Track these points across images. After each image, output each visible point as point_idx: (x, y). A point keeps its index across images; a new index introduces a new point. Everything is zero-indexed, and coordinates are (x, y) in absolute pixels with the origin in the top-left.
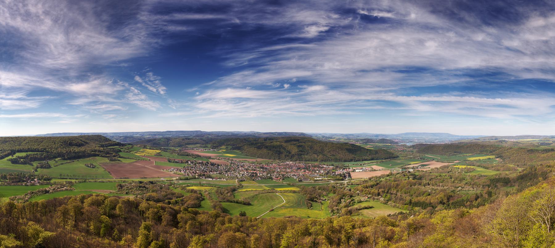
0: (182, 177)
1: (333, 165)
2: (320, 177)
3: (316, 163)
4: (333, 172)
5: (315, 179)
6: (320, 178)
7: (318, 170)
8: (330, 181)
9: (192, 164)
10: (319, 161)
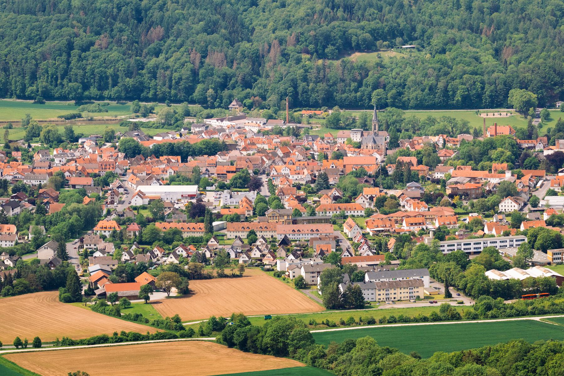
2: (538, 256)
5: (493, 275)
6: (536, 273)
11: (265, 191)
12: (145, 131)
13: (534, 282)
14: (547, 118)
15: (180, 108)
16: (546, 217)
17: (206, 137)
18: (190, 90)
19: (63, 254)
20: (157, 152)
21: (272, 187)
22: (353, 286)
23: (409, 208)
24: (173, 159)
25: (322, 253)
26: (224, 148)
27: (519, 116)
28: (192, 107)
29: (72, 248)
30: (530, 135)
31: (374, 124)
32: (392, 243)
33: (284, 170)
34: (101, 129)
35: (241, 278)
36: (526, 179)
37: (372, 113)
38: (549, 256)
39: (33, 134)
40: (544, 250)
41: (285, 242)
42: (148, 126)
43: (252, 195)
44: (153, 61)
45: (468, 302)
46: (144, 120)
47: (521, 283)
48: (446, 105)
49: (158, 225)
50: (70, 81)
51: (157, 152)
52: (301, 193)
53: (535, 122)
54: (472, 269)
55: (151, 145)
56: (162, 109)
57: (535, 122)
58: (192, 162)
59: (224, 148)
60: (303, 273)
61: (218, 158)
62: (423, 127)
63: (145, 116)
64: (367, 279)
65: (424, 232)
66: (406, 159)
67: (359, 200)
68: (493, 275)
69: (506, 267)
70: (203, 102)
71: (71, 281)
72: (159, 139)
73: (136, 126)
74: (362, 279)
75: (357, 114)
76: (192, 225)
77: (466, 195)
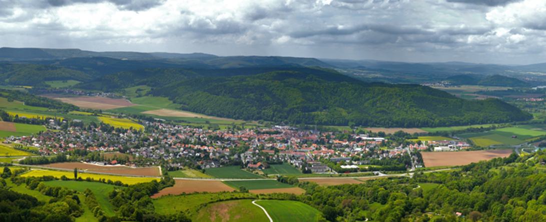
0: (35, 157)
1: (381, 135)
2: (353, 162)
3: (347, 129)
4: (383, 152)
5: (343, 167)
6: (353, 167)
7: (347, 146)
8: (376, 172)
9: (58, 127)
10: (350, 123)
11: (289, 144)
12: (261, 128)
13: (352, 169)
14: (357, 129)
15: (269, 122)
16: (356, 153)
17: (275, 130)
18: (272, 118)
19: (239, 156)
20: (264, 133)
21: (291, 143)
22: (331, 158)
23: (323, 149)
24: (267, 135)
25: (302, 160)
26: (280, 133)
27: (350, 128)
28: (272, 122)
29: (242, 155)
30: (353, 133)
31: (316, 129)
32: (319, 158)
33: (294, 139)
34: (250, 127)
35: (80, 218)
36: (352, 143)
37: (315, 126)
38: (356, 163)
39: (235, 127)
40: (355, 161)
41: (293, 156)
42: (262, 126)
43: (286, 145)
44: (263, 111)
45: (336, 173)
46: (261, 125)
47: (349, 169)
48: (334, 124)
49: (263, 151)
50: (340, 132)
51: (264, 133)
52: (298, 145)
53: (355, 130)
54: (337, 165)
55: (262, 131)
56: (266, 122)
57: (355, 130)
58: (272, 136)
59: (280, 133)
60: (297, 164)
61: (278, 135)
62: (328, 130)
63: (261, 124)
64: (312, 166)
65: (326, 156)
66: (323, 138)
67: (311, 147)
68: (343, 167)
69: (346, 165)
70: (275, 121)
71: (9, 204)
72: (264, 130)
73: (259, 127)
74: (311, 166)
75: (311, 126)
76: (271, 151)
77: (337, 147)
